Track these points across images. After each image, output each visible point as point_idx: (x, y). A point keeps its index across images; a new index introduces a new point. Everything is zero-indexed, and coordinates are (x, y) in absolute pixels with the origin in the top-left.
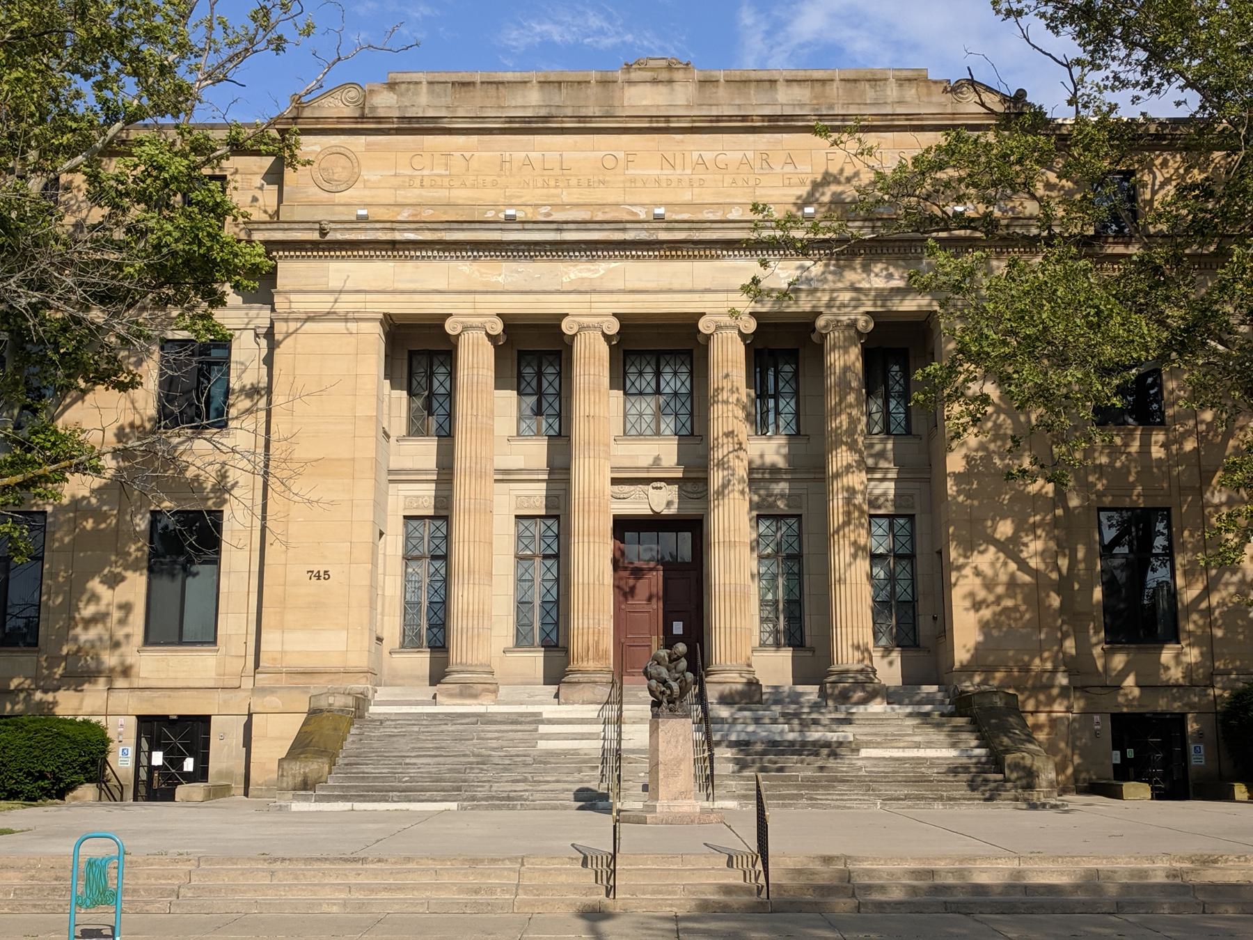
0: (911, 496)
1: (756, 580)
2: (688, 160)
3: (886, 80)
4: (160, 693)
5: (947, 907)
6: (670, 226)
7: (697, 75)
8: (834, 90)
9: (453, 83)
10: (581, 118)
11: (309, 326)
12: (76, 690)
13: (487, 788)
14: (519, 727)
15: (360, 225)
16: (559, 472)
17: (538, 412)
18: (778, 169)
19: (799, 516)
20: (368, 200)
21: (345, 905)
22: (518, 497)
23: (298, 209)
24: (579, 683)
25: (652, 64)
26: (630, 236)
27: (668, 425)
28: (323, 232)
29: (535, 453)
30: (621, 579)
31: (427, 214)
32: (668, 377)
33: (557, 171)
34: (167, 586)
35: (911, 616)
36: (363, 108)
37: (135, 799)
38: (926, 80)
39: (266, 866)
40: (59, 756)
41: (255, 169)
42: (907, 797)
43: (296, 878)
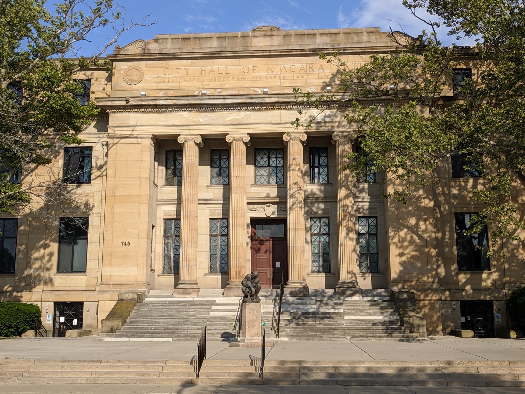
0: (376, 208)
1: (310, 244)
2: (279, 68)
3: (362, 32)
4: (63, 293)
5: (337, 383)
6: (270, 96)
7: (283, 33)
8: (340, 37)
9: (182, 39)
10: (233, 52)
11: (122, 140)
12: (30, 291)
13: (186, 332)
14: (204, 307)
15: (142, 99)
16: (226, 199)
17: (219, 174)
18: (316, 71)
19: (328, 218)
20: (146, 88)
21: (87, 380)
22: (210, 210)
23: (118, 92)
24: (232, 288)
25: (264, 28)
26: (254, 101)
27: (273, 180)
28: (127, 102)
29: (218, 192)
30: (254, 245)
31: (171, 93)
32: (273, 160)
33: (224, 74)
34: (67, 248)
35: (374, 258)
36: (144, 50)
37: (54, 336)
38: (380, 32)
39: (61, 364)
40: (18, 318)
41: (102, 76)
42: (361, 336)
43: (72, 369)
